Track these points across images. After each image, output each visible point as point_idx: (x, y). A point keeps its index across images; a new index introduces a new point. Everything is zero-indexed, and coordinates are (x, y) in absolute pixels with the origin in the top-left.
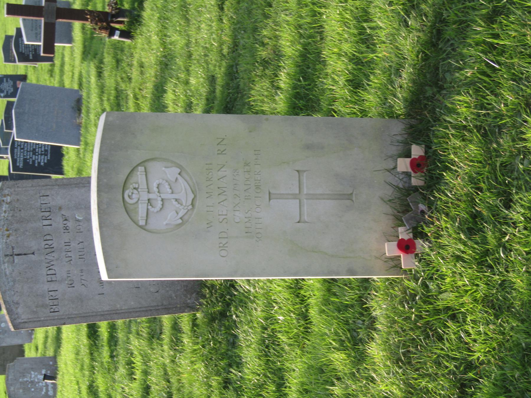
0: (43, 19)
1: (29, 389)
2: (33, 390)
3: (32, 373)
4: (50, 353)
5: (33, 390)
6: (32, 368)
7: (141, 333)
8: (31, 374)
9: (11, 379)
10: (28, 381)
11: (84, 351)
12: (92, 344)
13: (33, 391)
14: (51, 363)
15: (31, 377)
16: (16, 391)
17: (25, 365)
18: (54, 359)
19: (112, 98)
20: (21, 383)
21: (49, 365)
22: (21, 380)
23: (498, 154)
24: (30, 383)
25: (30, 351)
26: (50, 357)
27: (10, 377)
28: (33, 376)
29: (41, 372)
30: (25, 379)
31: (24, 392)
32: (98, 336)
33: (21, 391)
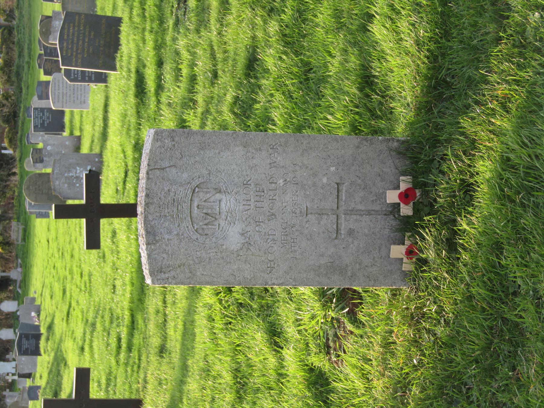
0: (83, 202)
1: (74, 185)
2: (78, 185)
3: (78, 168)
4: (97, 150)
5: (78, 185)
6: (78, 164)
7: (189, 27)
8: (77, 170)
9: (57, 173)
10: (73, 176)
11: (131, 111)
12: (139, 103)
13: (78, 187)
14: (97, 160)
15: (76, 173)
16: (61, 185)
17: (71, 161)
18: (100, 155)
19: (144, 236)
20: (66, 177)
21: (94, 161)
22: (66, 175)
23: (508, 241)
24: (75, 178)
25: (61, 337)
26: (96, 154)
27: (55, 172)
28: (78, 171)
29: (87, 168)
30: (71, 174)
31: (69, 187)
32: (145, 93)
33: (66, 185)
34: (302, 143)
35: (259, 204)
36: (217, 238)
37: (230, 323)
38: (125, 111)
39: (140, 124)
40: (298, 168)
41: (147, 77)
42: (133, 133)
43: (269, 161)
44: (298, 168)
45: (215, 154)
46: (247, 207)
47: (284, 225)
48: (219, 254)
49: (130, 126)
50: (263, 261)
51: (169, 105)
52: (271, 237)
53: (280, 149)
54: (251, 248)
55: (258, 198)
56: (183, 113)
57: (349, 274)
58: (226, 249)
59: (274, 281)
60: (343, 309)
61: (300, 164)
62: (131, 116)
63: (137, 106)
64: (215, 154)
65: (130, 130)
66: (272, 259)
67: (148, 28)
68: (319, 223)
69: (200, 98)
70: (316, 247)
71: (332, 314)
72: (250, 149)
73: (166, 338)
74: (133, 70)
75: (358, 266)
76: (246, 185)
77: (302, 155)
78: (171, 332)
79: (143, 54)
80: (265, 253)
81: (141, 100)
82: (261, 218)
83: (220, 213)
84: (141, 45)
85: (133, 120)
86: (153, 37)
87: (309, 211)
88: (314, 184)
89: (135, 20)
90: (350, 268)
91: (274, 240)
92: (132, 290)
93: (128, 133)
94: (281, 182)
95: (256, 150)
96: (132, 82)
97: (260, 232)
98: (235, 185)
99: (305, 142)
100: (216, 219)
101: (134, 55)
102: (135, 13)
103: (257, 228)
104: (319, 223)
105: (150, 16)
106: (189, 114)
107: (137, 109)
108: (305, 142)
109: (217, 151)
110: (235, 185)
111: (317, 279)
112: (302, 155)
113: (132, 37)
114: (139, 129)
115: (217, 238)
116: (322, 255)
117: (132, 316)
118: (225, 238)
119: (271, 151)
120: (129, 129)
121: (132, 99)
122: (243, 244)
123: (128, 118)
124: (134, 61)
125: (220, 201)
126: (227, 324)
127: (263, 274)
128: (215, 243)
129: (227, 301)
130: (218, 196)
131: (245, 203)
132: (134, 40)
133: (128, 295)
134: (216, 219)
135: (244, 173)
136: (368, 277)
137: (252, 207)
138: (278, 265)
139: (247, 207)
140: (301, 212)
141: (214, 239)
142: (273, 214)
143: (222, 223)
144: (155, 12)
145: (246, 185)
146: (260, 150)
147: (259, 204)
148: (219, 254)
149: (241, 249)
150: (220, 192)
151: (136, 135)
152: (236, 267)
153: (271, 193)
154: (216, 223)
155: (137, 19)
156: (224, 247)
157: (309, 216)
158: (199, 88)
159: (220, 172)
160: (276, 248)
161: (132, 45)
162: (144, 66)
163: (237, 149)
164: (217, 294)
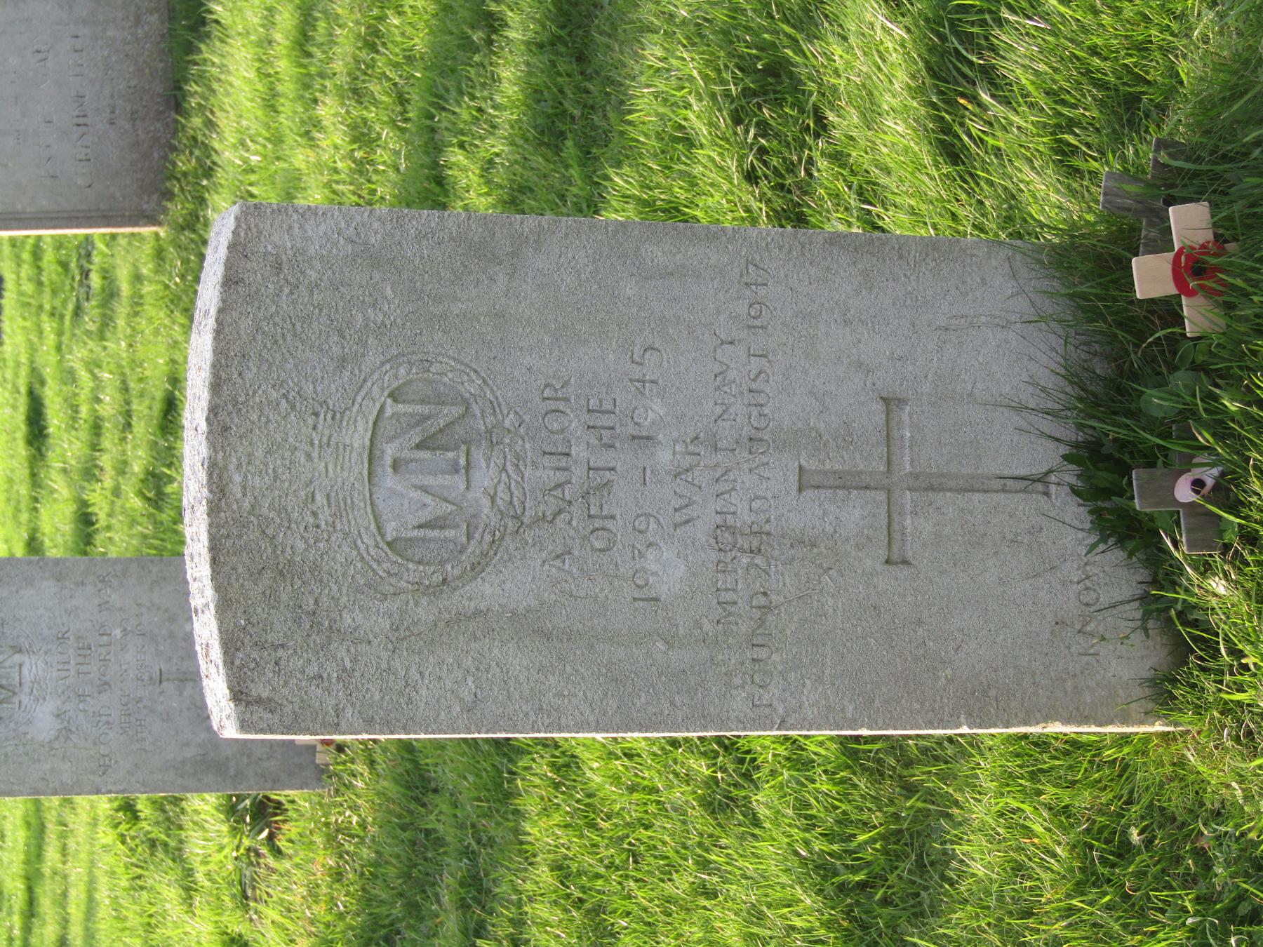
11: (23, 473)
34: (150, 572)
35: (83, 668)
36: (17, 723)
37: (139, 877)
38: (13, 471)
39: (36, 500)
40: (144, 610)
41: (47, 402)
42: (24, 517)
43: (96, 601)
44: (144, 610)
45: (11, 592)
46: (64, 674)
47: (124, 700)
48: (21, 748)
49: (19, 502)
50: (92, 757)
51: (65, 471)
52: (104, 718)
53: (115, 583)
54: (72, 736)
55: (81, 660)
56: (83, 488)
57: (232, 772)
58: (33, 739)
59: (110, 787)
60: (261, 831)
61: (148, 604)
62: (21, 482)
63: (30, 462)
64: (11, 592)
65: (20, 511)
66: (106, 752)
67: (47, 307)
68: (181, 695)
69: (106, 461)
70: (177, 732)
71: (246, 842)
72: (67, 583)
73: (67, 921)
74: (23, 390)
75: (245, 760)
76: (62, 639)
77: (151, 589)
78: (72, 909)
79: (39, 361)
80: (95, 744)
81: (39, 450)
82: (87, 690)
83: (20, 684)
84: (36, 340)
85: (24, 490)
86: (55, 325)
87: (165, 677)
88: (172, 635)
89: (24, 288)
90: (232, 763)
91: (108, 723)
92: (28, 838)
93: (15, 517)
94: (118, 632)
95: (77, 584)
96: (20, 417)
97: (85, 711)
98: (44, 639)
99: (155, 570)
100: (14, 693)
101: (23, 359)
102: (23, 274)
103: (81, 706)
104: (181, 695)
105: (52, 283)
106: (94, 491)
107: (31, 468)
108: (155, 570)
109: (14, 589)
110: (44, 639)
111: (180, 781)
112: (151, 589)
113: (20, 321)
114: (36, 509)
115: (17, 723)
116: (187, 745)
117: (30, 890)
118: (29, 722)
119: (100, 585)
120: (18, 510)
121: (22, 450)
122: (60, 731)
123: (15, 487)
124: (24, 372)
125: (20, 666)
126: (133, 879)
127: (92, 777)
128: (14, 730)
129: (133, 838)
130: (17, 658)
131: (60, 667)
132: (24, 328)
133: (21, 847)
134: (14, 693)
135: (59, 621)
136: (263, 776)
137: (72, 672)
138: (116, 762)
139: (64, 674)
140: (151, 678)
141: (12, 725)
142: (106, 683)
143: (25, 699)
144: (58, 274)
145: (62, 639)
146: (83, 584)
147: (83, 668)
148: (21, 748)
149: (57, 738)
150: (20, 651)
151: (30, 521)
152: (48, 767)
153: (103, 650)
154: (16, 700)
155: (29, 288)
156: (29, 737)
157: (165, 684)
158: (106, 442)
159: (18, 620)
160: (111, 735)
161: (20, 339)
162: (43, 383)
163: (45, 584)
164: (116, 826)
